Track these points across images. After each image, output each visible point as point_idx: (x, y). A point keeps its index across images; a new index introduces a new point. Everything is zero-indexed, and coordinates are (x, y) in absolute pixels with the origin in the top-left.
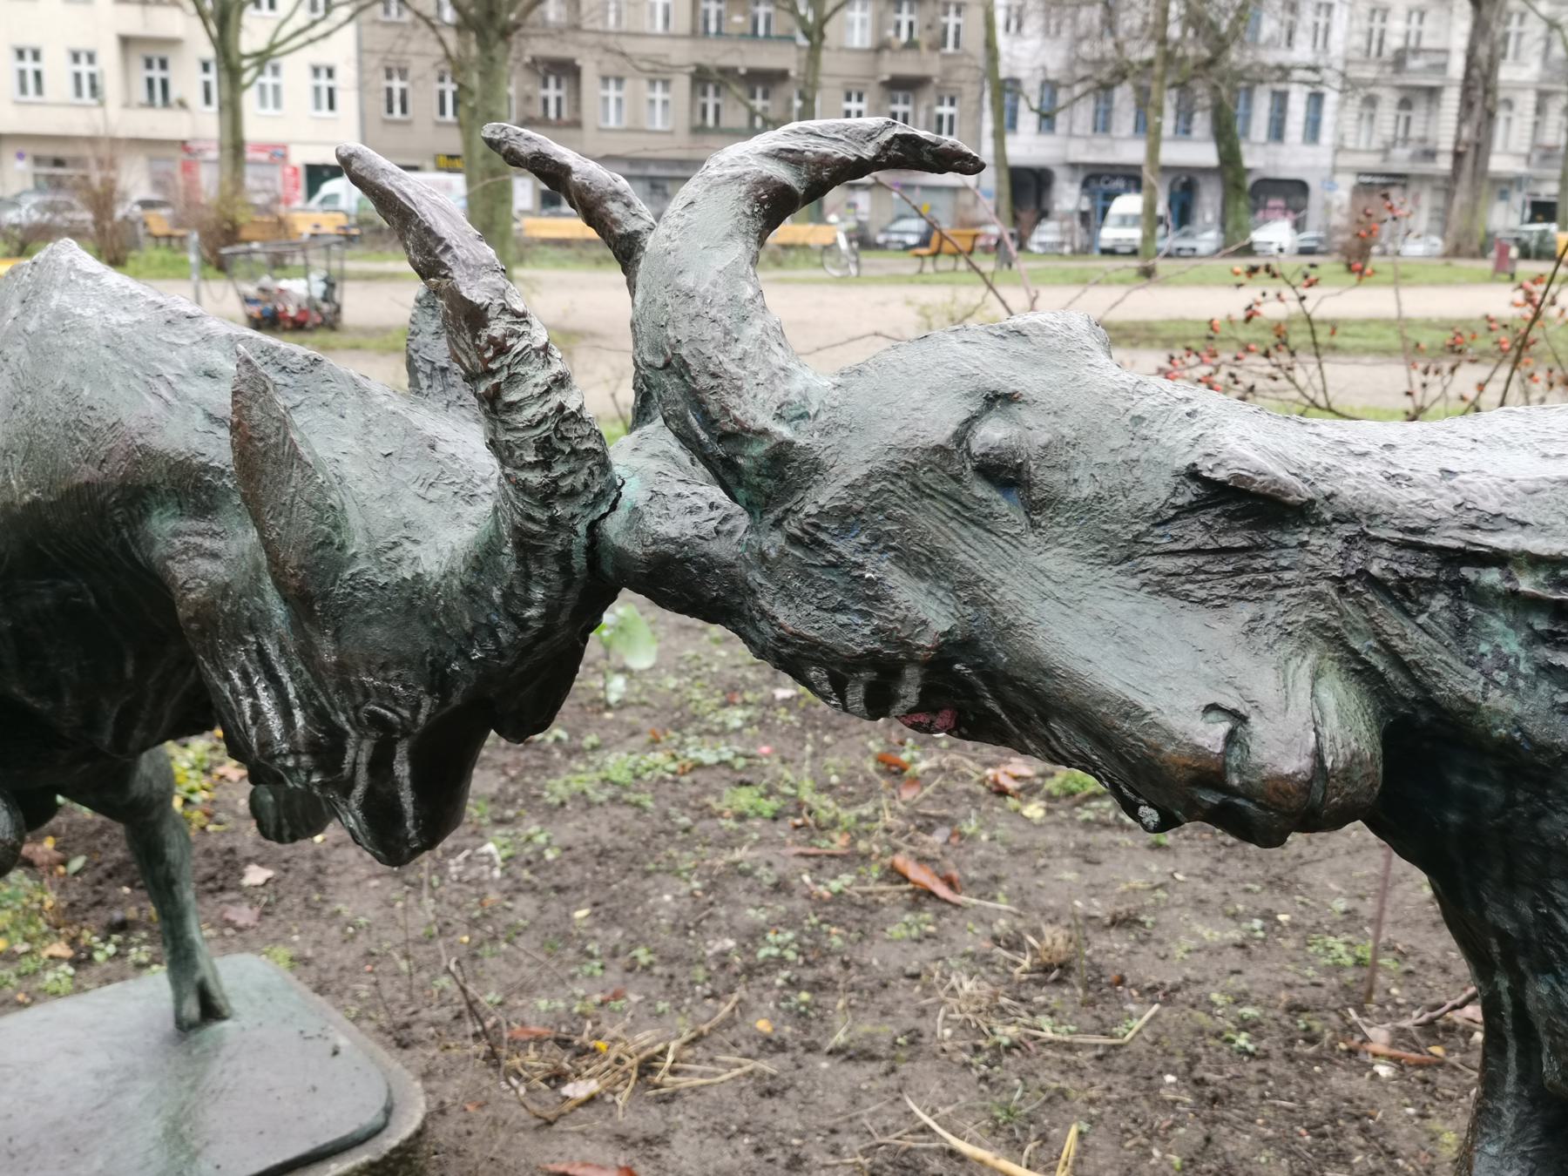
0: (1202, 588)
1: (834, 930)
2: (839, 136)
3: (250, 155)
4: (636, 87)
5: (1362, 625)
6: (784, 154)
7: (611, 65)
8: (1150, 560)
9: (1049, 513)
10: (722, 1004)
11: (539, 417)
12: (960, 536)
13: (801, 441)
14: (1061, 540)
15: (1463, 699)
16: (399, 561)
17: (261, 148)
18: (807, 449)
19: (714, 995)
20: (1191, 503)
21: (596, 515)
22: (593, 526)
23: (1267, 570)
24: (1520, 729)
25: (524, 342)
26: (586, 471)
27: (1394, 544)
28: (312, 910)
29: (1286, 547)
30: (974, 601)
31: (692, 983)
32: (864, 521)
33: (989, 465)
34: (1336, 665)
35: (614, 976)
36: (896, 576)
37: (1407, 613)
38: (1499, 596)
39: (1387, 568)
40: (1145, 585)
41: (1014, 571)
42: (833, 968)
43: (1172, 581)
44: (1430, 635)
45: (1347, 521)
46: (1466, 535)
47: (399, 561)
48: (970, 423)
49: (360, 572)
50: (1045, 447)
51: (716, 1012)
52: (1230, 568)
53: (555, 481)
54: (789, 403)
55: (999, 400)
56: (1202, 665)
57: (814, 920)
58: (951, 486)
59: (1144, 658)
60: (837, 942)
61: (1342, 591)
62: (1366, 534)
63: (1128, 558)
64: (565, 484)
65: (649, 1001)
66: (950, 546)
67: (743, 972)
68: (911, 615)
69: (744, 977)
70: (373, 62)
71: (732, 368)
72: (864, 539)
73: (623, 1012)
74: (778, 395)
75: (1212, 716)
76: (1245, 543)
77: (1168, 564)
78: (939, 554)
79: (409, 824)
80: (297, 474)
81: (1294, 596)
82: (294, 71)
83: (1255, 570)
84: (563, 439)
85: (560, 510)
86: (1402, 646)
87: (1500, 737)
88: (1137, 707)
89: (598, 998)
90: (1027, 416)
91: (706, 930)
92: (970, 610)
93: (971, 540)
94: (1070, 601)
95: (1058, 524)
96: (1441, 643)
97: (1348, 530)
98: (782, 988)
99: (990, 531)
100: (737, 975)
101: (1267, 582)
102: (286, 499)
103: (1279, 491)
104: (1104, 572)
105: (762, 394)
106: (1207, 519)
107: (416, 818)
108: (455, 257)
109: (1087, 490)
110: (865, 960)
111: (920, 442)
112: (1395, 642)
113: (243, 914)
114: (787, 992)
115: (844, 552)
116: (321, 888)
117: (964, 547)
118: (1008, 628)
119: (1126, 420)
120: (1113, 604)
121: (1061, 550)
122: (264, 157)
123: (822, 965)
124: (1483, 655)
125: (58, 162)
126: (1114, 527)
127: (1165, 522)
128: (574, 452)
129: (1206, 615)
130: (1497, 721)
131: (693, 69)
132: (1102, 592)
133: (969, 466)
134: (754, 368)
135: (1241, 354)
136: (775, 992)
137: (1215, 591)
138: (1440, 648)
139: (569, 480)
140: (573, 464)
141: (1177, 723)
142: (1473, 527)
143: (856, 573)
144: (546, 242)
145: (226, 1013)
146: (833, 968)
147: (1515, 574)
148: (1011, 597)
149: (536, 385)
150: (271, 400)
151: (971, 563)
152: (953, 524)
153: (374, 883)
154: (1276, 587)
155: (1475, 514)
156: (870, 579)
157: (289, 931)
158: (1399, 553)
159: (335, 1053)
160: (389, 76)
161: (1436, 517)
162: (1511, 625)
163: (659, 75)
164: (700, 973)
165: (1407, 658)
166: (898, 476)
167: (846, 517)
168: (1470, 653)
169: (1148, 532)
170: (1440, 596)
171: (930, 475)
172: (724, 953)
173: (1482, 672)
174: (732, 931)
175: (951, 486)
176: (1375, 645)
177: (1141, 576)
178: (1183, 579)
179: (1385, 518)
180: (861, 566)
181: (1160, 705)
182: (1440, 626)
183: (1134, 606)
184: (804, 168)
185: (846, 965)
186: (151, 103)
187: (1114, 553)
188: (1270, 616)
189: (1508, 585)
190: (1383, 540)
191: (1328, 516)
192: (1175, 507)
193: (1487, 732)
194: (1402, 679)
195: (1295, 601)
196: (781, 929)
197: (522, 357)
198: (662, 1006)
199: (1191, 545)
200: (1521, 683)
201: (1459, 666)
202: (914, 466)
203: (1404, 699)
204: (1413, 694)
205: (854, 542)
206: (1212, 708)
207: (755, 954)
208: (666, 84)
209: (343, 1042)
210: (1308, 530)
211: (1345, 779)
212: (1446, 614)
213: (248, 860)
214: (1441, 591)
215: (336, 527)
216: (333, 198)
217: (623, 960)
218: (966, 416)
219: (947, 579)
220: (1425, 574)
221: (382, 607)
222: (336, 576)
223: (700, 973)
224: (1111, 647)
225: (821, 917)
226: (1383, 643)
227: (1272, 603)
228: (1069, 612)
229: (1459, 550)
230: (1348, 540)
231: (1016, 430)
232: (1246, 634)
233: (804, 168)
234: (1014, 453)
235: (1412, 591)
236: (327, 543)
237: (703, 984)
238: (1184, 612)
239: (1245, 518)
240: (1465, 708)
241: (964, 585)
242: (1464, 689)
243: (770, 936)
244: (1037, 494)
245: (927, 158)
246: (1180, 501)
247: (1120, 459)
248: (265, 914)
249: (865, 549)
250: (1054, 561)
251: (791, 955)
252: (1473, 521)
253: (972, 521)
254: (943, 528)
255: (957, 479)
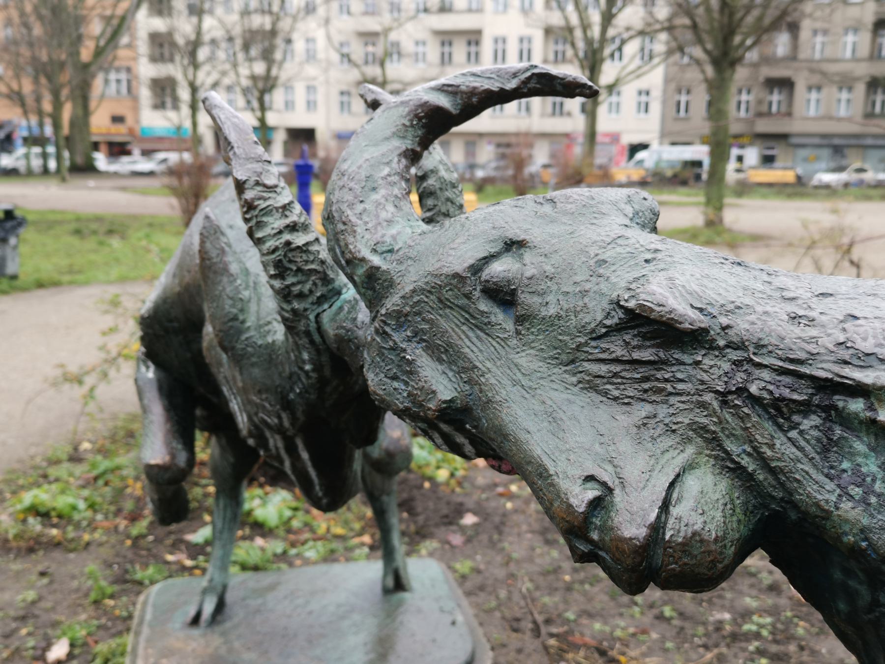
0: (617, 389)
1: (802, 623)
2: (492, 76)
3: (599, 139)
4: (830, 92)
5: (739, 432)
6: (446, 88)
7: (816, 79)
8: (585, 364)
9: (527, 325)
10: (708, 653)
11: (273, 247)
12: (468, 337)
13: (384, 267)
14: (533, 345)
15: (817, 505)
16: (269, 332)
17: (607, 135)
18: (387, 272)
19: (706, 647)
20: (617, 324)
21: (320, 310)
22: (318, 316)
23: (666, 380)
24: (866, 539)
25: (268, 203)
26: (311, 282)
27: (775, 370)
28: (492, 544)
29: (684, 364)
30: (469, 382)
31: (694, 636)
32: (409, 321)
33: (489, 289)
34: (712, 461)
35: (647, 619)
36: (424, 360)
37: (780, 427)
38: (861, 422)
39: (764, 389)
40: (580, 382)
41: (499, 363)
42: (792, 648)
43: (598, 381)
44: (797, 448)
45: (737, 348)
46: (837, 369)
47: (269, 332)
48: (489, 259)
49: (251, 337)
50: (530, 278)
51: (702, 656)
52: (638, 376)
53: (288, 287)
54: (383, 243)
55: (513, 246)
56: (597, 446)
57: (789, 614)
58: (463, 301)
59: (561, 435)
60: (800, 631)
61: (724, 403)
62: (752, 360)
63: (573, 362)
64: (296, 289)
65: (663, 639)
66: (459, 342)
67: (729, 636)
68: (426, 386)
69: (728, 640)
70: (673, 86)
71: (353, 219)
72: (409, 334)
73: (644, 642)
74: (377, 237)
75: (589, 485)
76: (652, 358)
77: (595, 368)
78: (452, 347)
79: (317, 488)
80: (225, 279)
81: (683, 402)
82: (629, 93)
83: (657, 380)
84: (290, 261)
85: (296, 305)
86: (769, 453)
87: (849, 543)
88: (546, 470)
89: (631, 630)
90: (528, 256)
91: (714, 604)
92: (467, 387)
93: (475, 340)
94: (530, 388)
95: (532, 333)
96: (806, 456)
97: (735, 355)
98: (752, 653)
99: (487, 334)
100: (724, 637)
101: (664, 389)
102: (217, 293)
103: (672, 319)
104: (556, 370)
105: (367, 236)
106: (627, 338)
107: (321, 485)
108: (235, 153)
109: (552, 310)
110: (817, 648)
111: (445, 271)
112: (764, 449)
113: (457, 539)
114: (755, 656)
115: (397, 340)
116: (500, 533)
117: (468, 343)
118: (488, 403)
119: (592, 262)
120: (556, 393)
121: (532, 352)
122: (607, 140)
123: (783, 644)
124: (844, 471)
125: (508, 145)
126: (565, 338)
127: (599, 338)
128: (299, 270)
129: (616, 409)
130: (847, 528)
131: (868, 79)
132: (551, 385)
133: (478, 289)
134: (367, 219)
135: (438, 192)
136: (747, 654)
137: (626, 393)
138: (805, 460)
139: (299, 287)
140: (300, 277)
141: (564, 484)
142: (846, 363)
143: (402, 355)
144: (760, 185)
145: (407, 587)
146: (792, 648)
147: (876, 405)
148: (493, 381)
149: (273, 229)
150: (218, 239)
151: (471, 355)
152: (464, 328)
153: (529, 536)
154: (671, 394)
155: (851, 351)
156: (408, 360)
157: (476, 553)
158: (778, 378)
159: (454, 623)
160: (679, 92)
161: (815, 351)
162: (872, 449)
163: (846, 83)
164: (701, 630)
165: (773, 464)
166: (430, 292)
167: (400, 318)
168: (832, 467)
169: (586, 344)
170: (813, 417)
171: (450, 293)
172: (721, 622)
173: (839, 486)
174: (731, 609)
175: (463, 301)
176: (749, 449)
177: (579, 375)
178: (605, 380)
179: (770, 348)
180: (404, 350)
181: (559, 470)
182: (808, 441)
183: (570, 396)
184: (459, 97)
185: (802, 648)
186: (554, 114)
187: (564, 357)
188: (661, 416)
189: (868, 414)
190: (766, 366)
191: (722, 343)
192: (606, 327)
193: (838, 538)
194: (770, 479)
195: (682, 406)
196: (764, 614)
197: (267, 211)
198: (669, 645)
199: (614, 355)
200: (873, 500)
201: (821, 478)
202: (440, 286)
203: (773, 497)
204: (781, 495)
205: (404, 335)
206: (590, 478)
207: (740, 626)
208: (850, 89)
209: (460, 618)
210: (703, 352)
211: (684, 551)
212: (815, 433)
213: (468, 511)
214: (814, 413)
215: (242, 310)
216: (641, 162)
217: (655, 611)
218: (486, 254)
219: (456, 365)
220: (796, 397)
221: (259, 357)
222: (238, 338)
223: (701, 630)
224: (546, 424)
225: (794, 613)
226: (755, 448)
227: (665, 406)
228: (527, 396)
229: (826, 380)
230: (737, 363)
231: (518, 265)
232: (639, 427)
233: (459, 97)
234: (509, 281)
235: (785, 410)
236: (235, 318)
237: (700, 637)
238: (602, 406)
239: (654, 338)
240: (819, 513)
241: (465, 370)
242: (819, 497)
243: (755, 618)
244: (520, 311)
245: (559, 88)
246: (608, 322)
247: (578, 289)
248: (469, 540)
249: (409, 340)
250: (527, 360)
251: (765, 633)
252: (847, 358)
253: (476, 326)
254: (457, 329)
255: (468, 296)
